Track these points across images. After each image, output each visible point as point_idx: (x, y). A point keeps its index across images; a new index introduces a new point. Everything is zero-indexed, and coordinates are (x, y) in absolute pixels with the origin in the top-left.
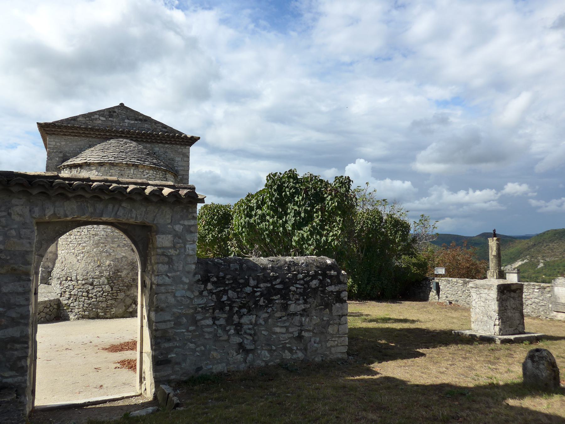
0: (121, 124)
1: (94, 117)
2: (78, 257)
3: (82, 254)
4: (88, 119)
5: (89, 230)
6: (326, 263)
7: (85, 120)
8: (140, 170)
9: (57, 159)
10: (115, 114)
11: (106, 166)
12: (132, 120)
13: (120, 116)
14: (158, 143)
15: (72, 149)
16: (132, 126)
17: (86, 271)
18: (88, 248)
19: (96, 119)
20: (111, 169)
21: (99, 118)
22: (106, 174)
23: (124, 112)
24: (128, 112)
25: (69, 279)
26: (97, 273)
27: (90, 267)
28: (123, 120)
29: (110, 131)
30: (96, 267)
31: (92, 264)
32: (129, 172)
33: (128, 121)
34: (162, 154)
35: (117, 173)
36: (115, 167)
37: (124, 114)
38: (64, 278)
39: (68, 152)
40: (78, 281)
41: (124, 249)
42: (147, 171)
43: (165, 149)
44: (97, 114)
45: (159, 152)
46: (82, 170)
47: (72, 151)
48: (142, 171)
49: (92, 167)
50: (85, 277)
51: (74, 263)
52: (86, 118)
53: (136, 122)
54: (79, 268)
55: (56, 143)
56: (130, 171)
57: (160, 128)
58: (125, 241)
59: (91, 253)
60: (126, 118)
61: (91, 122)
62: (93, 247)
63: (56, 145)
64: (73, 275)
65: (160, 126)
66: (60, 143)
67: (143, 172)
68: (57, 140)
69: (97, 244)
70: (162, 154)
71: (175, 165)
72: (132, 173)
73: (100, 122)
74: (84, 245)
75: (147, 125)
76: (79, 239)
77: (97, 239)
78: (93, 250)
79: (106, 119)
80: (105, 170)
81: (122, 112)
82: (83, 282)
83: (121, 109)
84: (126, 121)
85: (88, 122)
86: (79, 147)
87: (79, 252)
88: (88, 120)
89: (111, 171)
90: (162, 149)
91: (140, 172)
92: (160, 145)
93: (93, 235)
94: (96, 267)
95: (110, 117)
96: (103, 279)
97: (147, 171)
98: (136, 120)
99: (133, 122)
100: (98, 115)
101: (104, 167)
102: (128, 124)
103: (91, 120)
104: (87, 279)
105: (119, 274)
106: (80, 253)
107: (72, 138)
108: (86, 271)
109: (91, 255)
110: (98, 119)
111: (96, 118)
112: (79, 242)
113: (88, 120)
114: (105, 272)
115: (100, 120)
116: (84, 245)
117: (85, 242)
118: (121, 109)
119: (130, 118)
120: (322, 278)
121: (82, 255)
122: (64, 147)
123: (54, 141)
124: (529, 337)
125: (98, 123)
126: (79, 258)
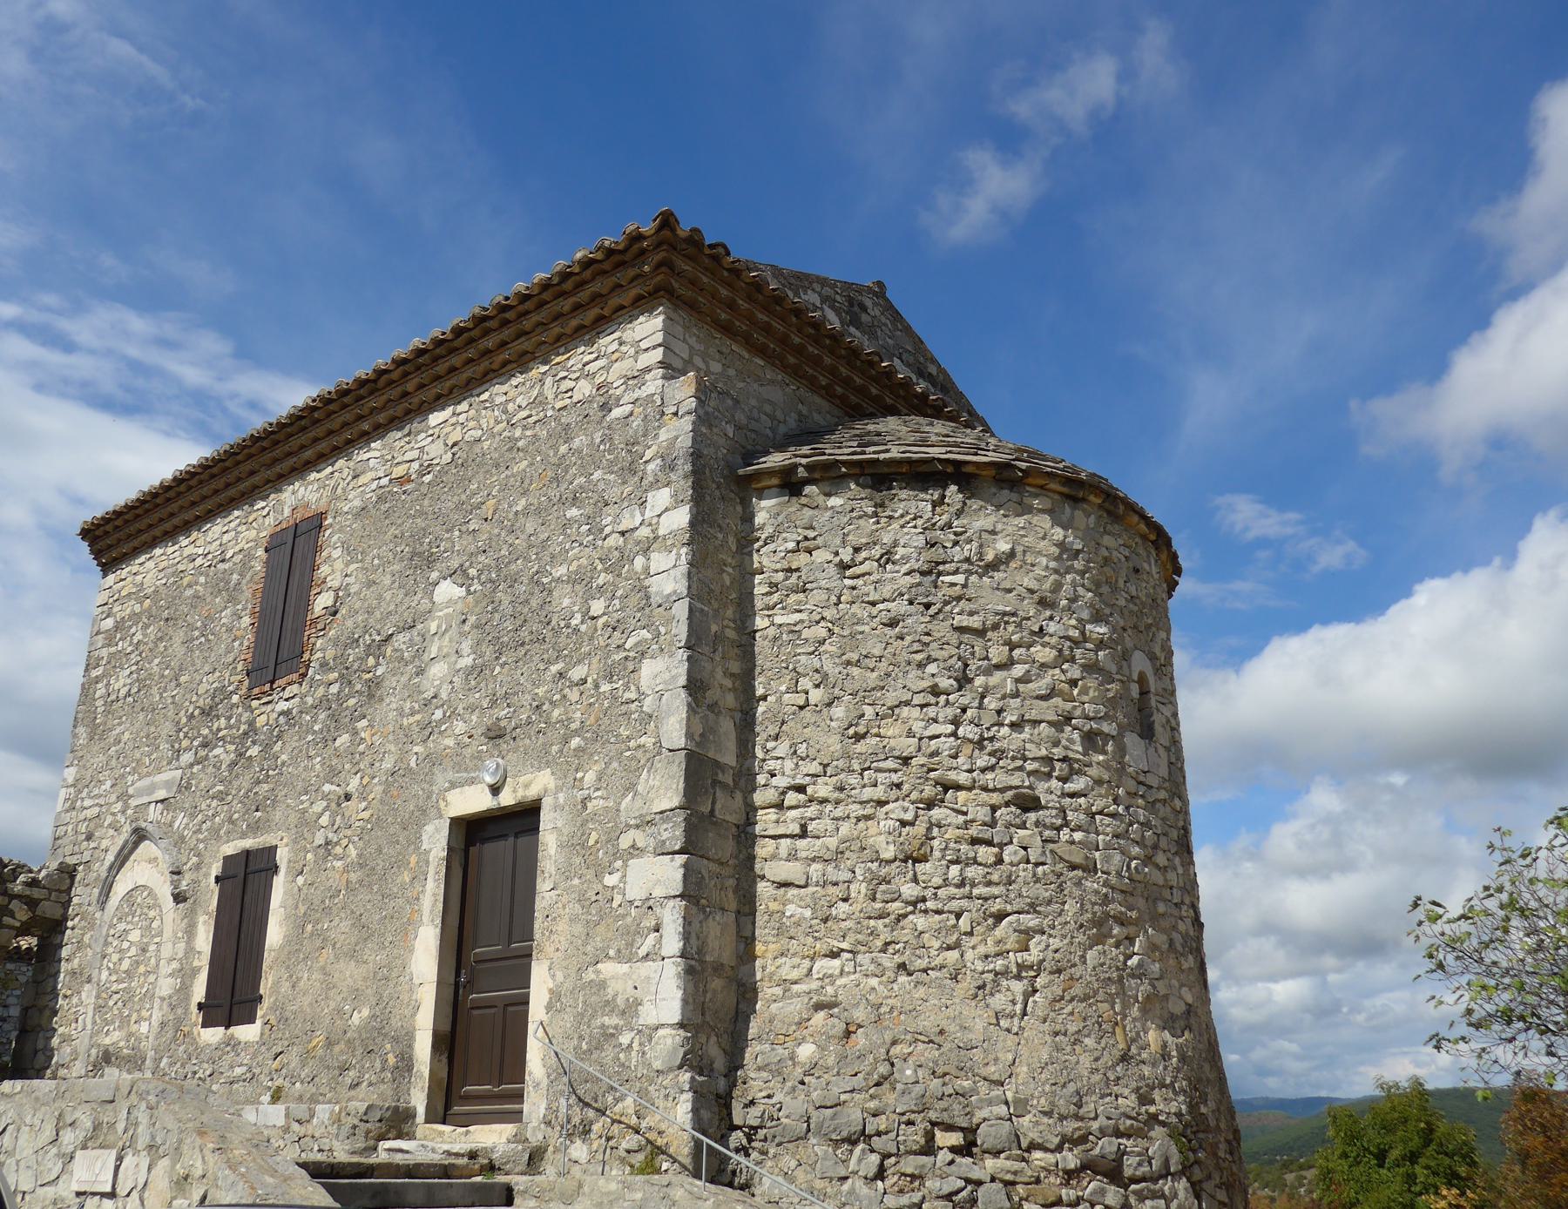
2: (990, 1000)
3: (1018, 977)
5: (1047, 833)
9: (730, 431)
17: (1071, 1087)
18: (1055, 943)
26: (1129, 1102)
27: (1086, 1061)
30: (1113, 1067)
31: (1089, 1042)
38: (915, 1137)
46: (974, 504)
50: (1070, 1126)
51: (975, 1036)
54: (1022, 1070)
59: (1077, 972)
62: (1080, 938)
64: (985, 1113)
69: (1099, 922)
74: (1030, 921)
76: (989, 884)
77: (1097, 892)
78: (1083, 958)
82: (1071, 1159)
87: (999, 964)
93: (1073, 867)
94: (1113, 1067)
96: (1159, 1143)
101: (1084, 511)
104: (1083, 1139)
106: (1005, 973)
108: (1071, 1087)
109: (1078, 990)
112: (997, 906)
114: (1157, 1095)
116: (1030, 921)
117: (1033, 908)
120: (1199, 1108)
121: (1018, 987)
124: (386, 1183)
126: (999, 1001)
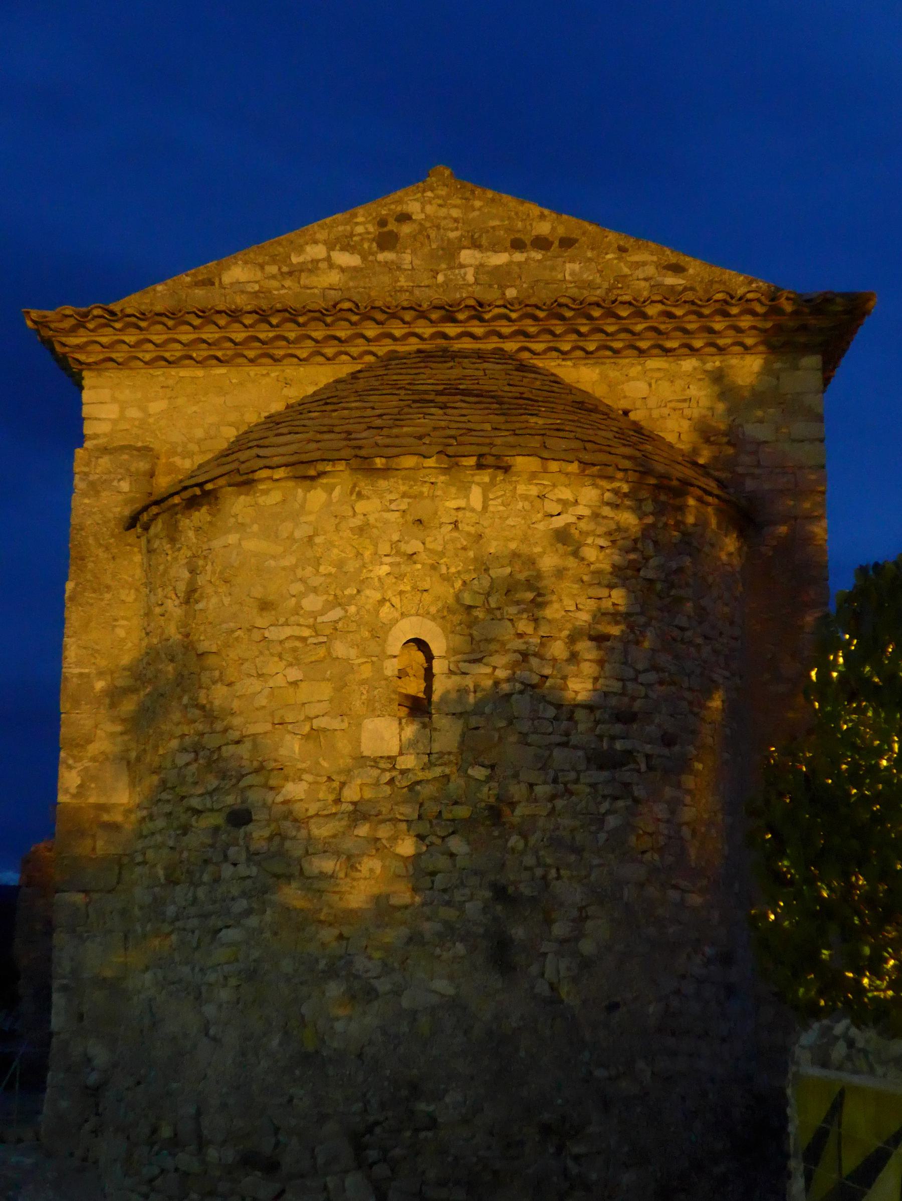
0: (440, 278)
1: (301, 259)
4: (273, 269)
6: (802, 769)
7: (259, 275)
8: (521, 489)
9: (125, 486)
10: (406, 229)
11: (332, 481)
12: (495, 247)
13: (433, 233)
14: (641, 352)
15: (199, 433)
16: (501, 276)
19: (313, 267)
20: (360, 495)
21: (328, 259)
22: (334, 521)
23: (455, 213)
24: (473, 209)
25: (341, 1083)
28: (450, 252)
29: (380, 316)
32: (462, 503)
33: (477, 254)
34: (666, 411)
35: (393, 517)
36: (383, 484)
37: (456, 220)
39: (179, 450)
40: (202, 1144)
41: (445, 955)
42: (566, 494)
43: (679, 384)
44: (316, 242)
45: (652, 402)
47: (199, 442)
48: (534, 491)
49: (266, 492)
52: (262, 267)
53: (519, 257)
55: (122, 410)
56: (467, 497)
57: (651, 270)
58: (448, 903)
60: (465, 243)
61: (288, 283)
63: (122, 417)
65: (644, 264)
66: (144, 409)
67: (542, 497)
68: (126, 394)
70: (666, 411)
71: (740, 470)
72: (478, 506)
73: (334, 278)
75: (576, 267)
79: (364, 258)
80: (329, 503)
81: (443, 212)
83: (438, 197)
84: (467, 256)
85: (274, 284)
86: (233, 417)
88: (274, 277)
89: (361, 506)
90: (665, 386)
91: (525, 498)
92: (653, 363)
95: (382, 247)
97: (566, 494)
98: (517, 245)
99: (500, 259)
100: (325, 243)
102: (476, 273)
103: (290, 273)
105: (422, 1106)
107: (200, 373)
110: (323, 265)
111: (316, 262)
113: (274, 277)
115: (331, 266)
118: (438, 197)
119: (484, 242)
122: (163, 423)
123: (114, 399)
125: (326, 285)
